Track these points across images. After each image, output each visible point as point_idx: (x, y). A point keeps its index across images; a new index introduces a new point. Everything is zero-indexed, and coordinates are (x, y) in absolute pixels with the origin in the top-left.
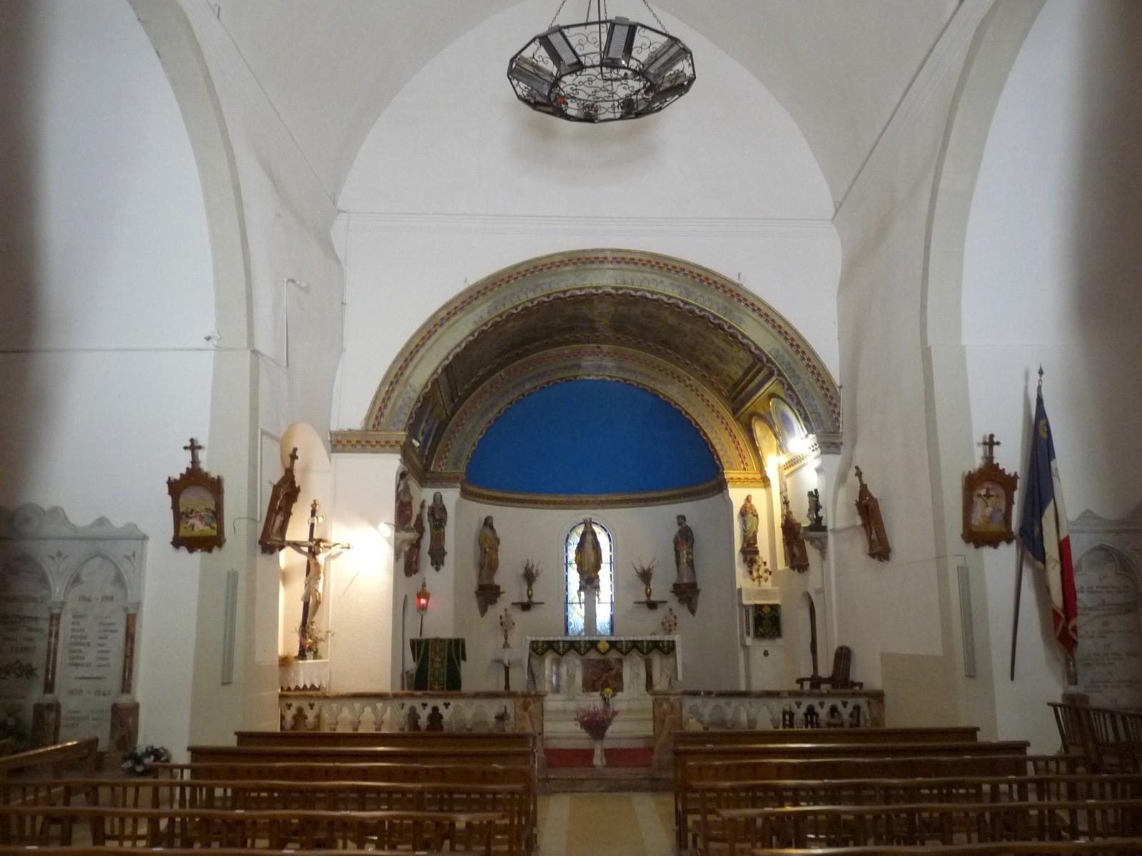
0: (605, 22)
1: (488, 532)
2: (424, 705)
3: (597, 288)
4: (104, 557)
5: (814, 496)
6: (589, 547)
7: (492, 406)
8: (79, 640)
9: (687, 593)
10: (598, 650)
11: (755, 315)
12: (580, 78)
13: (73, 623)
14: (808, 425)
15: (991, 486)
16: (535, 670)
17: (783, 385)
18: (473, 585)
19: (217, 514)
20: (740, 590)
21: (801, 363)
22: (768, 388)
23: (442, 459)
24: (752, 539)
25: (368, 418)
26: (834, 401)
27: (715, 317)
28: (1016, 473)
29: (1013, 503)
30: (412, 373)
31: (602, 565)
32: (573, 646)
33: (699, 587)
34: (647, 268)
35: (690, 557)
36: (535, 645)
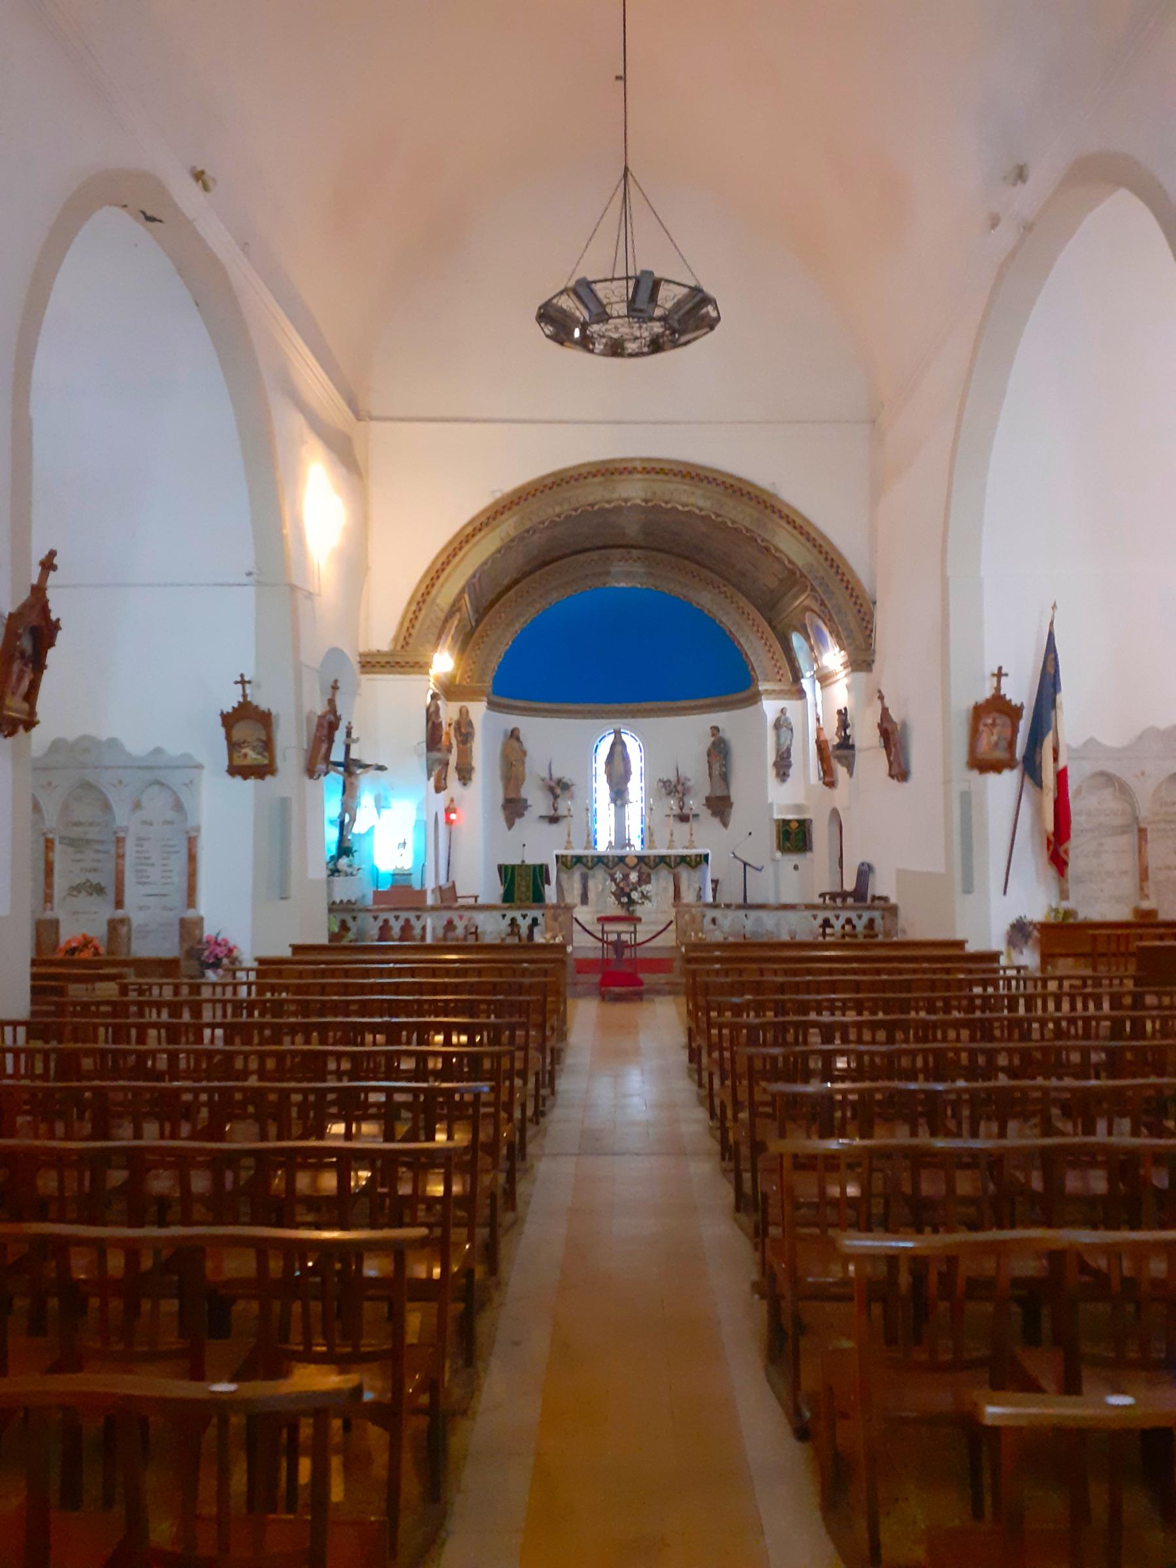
2: (524, 917)
3: (626, 500)
4: (162, 784)
5: (843, 714)
6: (617, 758)
8: (144, 861)
9: (720, 806)
10: (627, 865)
12: (606, 327)
13: (138, 845)
14: (841, 642)
16: (565, 885)
17: (817, 600)
19: (267, 745)
20: (771, 805)
22: (803, 601)
25: (396, 639)
27: (748, 530)
28: (1022, 704)
29: (1018, 731)
30: (439, 592)
32: (600, 860)
33: (732, 799)
34: (678, 479)
35: (724, 770)
36: (564, 860)
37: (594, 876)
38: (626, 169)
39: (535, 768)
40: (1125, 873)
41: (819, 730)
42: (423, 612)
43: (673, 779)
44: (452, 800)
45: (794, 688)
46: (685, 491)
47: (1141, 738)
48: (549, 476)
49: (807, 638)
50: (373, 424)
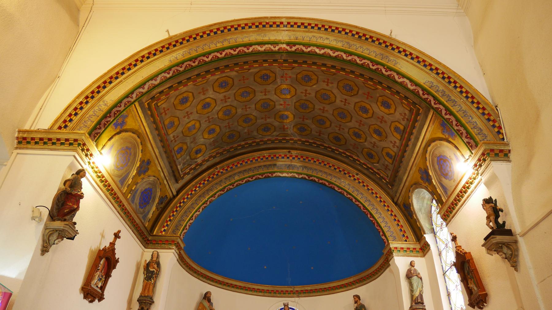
1: (206, 304)
7: (208, 191)
21: (454, 91)
23: (164, 227)
24: (419, 299)
45: (418, 247)
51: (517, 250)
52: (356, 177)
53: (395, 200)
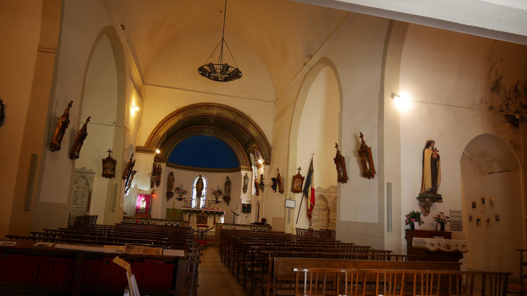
0: (222, 65)
4: (84, 177)
5: (262, 176)
6: (200, 184)
9: (227, 199)
10: (201, 213)
11: (252, 126)
13: (75, 193)
15: (298, 179)
18: (166, 192)
19: (114, 169)
25: (146, 144)
26: (270, 152)
27: (242, 125)
30: (159, 132)
31: (203, 189)
34: (226, 110)
37: (192, 216)
38: (223, 38)
39: (176, 185)
40: (324, 220)
41: (256, 180)
42: (155, 137)
43: (217, 190)
44: (153, 191)
45: (250, 168)
46: (227, 113)
47: (330, 187)
48: (192, 105)
49: (254, 155)
50: (147, 86)
51: (264, 188)
52: (233, 139)
53: (246, 150)
